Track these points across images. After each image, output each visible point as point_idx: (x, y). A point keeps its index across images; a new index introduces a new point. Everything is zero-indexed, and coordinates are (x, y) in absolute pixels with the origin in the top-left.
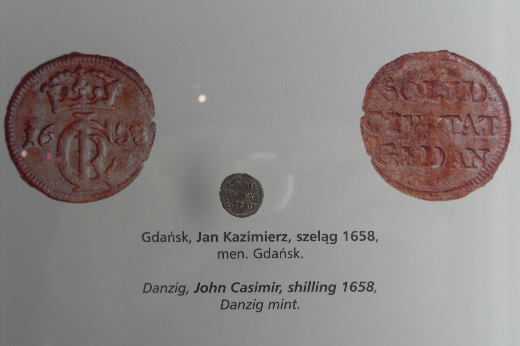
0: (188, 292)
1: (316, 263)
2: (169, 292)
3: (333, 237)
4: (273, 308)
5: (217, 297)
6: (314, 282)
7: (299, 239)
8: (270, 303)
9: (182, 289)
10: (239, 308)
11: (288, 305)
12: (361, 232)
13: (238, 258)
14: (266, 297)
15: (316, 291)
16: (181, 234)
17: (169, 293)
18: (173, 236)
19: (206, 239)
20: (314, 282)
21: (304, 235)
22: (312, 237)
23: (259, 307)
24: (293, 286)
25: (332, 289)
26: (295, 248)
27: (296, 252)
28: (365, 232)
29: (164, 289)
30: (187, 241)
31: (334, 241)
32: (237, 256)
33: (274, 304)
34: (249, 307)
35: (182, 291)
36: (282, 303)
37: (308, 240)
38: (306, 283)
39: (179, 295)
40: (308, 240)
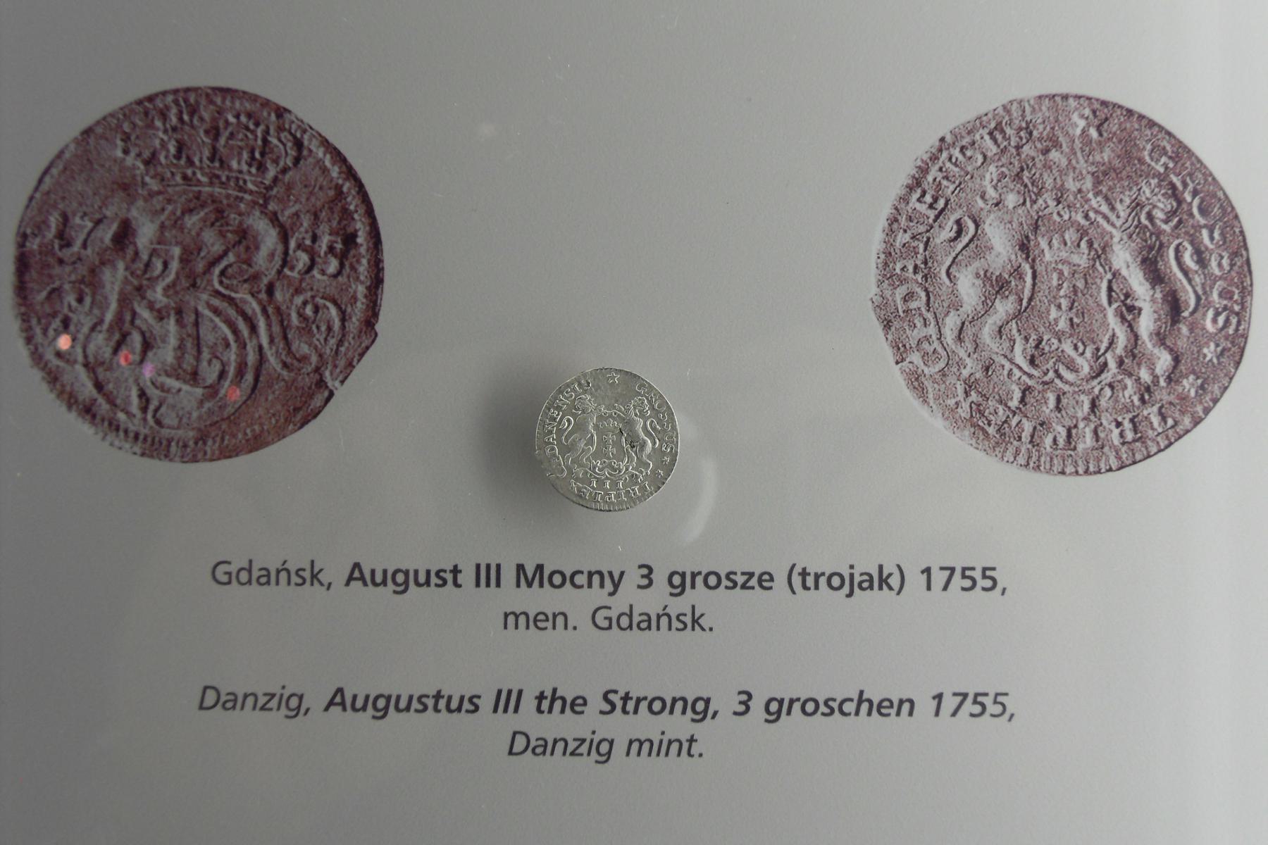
0: (307, 710)
1: (747, 645)
2: (572, 754)
4: (639, 754)
5: (494, 728)
8: (631, 742)
9: (294, 702)
11: (675, 746)
12: (985, 569)
13: (554, 628)
14: (620, 727)
16: (308, 567)
18: (288, 571)
19: (865, 585)
21: (743, 574)
23: (602, 750)
26: (693, 607)
27: (697, 616)
28: (973, 569)
29: (250, 700)
30: (322, 584)
31: (678, 591)
32: (549, 624)
33: (641, 744)
34: (578, 751)
35: (295, 706)
36: (661, 741)
37: (753, 588)
40: (753, 588)
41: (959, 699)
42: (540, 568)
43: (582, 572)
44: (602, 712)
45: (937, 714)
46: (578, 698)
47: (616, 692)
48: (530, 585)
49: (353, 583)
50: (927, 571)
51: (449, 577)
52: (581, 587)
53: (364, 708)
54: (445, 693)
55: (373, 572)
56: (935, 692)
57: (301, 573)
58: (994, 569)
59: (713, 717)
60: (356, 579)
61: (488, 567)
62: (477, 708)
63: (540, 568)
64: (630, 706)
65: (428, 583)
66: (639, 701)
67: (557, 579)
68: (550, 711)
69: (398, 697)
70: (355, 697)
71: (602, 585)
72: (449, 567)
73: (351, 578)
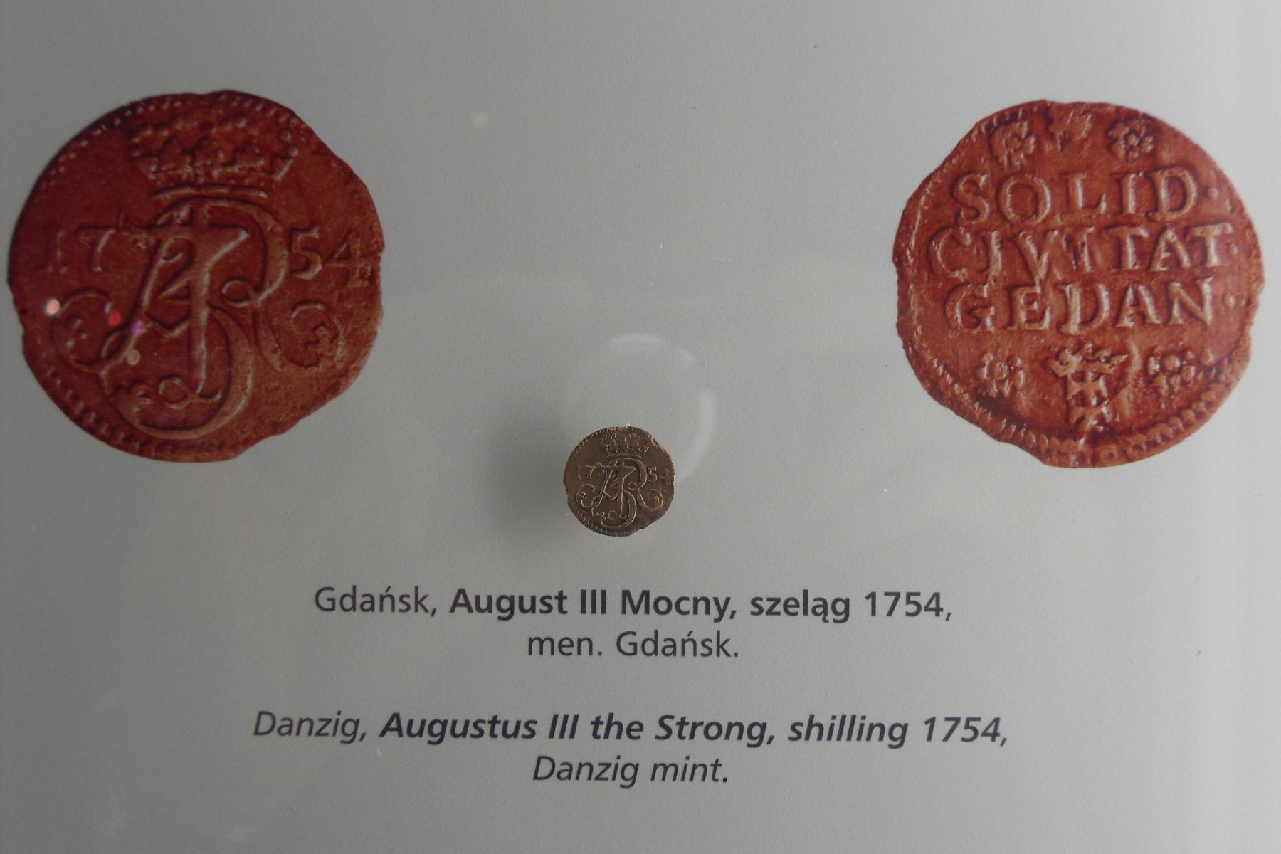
0: (363, 735)
1: (777, 671)
3: (840, 607)
4: (664, 779)
5: (523, 752)
6: (854, 718)
7: (756, 610)
8: (656, 767)
9: (350, 728)
10: (577, 778)
11: (700, 771)
13: (579, 653)
15: (859, 738)
17: (319, 738)
20: (854, 718)
21: (769, 599)
22: (790, 606)
23: (627, 775)
24: (801, 724)
25: (897, 735)
30: (426, 611)
33: (666, 768)
34: (324, 731)
35: (350, 731)
36: (686, 766)
37: (778, 614)
38: (834, 718)
39: (342, 742)
40: (778, 614)
41: (951, 723)
42: (646, 594)
43: (687, 599)
44: (658, 738)
45: (929, 738)
46: (632, 724)
47: (672, 717)
48: (635, 611)
49: (457, 609)
50: (872, 596)
51: (554, 603)
52: (687, 613)
53: (420, 734)
54: (501, 718)
55: (478, 598)
56: (928, 718)
57: (405, 599)
58: (918, 594)
59: (769, 742)
60: (461, 605)
61: (594, 593)
62: (533, 733)
63: (646, 594)
64: (687, 731)
65: (533, 609)
66: (695, 726)
67: (663, 606)
68: (607, 736)
69: (455, 723)
70: (411, 722)
71: (708, 612)
72: (555, 593)
73: (456, 604)
